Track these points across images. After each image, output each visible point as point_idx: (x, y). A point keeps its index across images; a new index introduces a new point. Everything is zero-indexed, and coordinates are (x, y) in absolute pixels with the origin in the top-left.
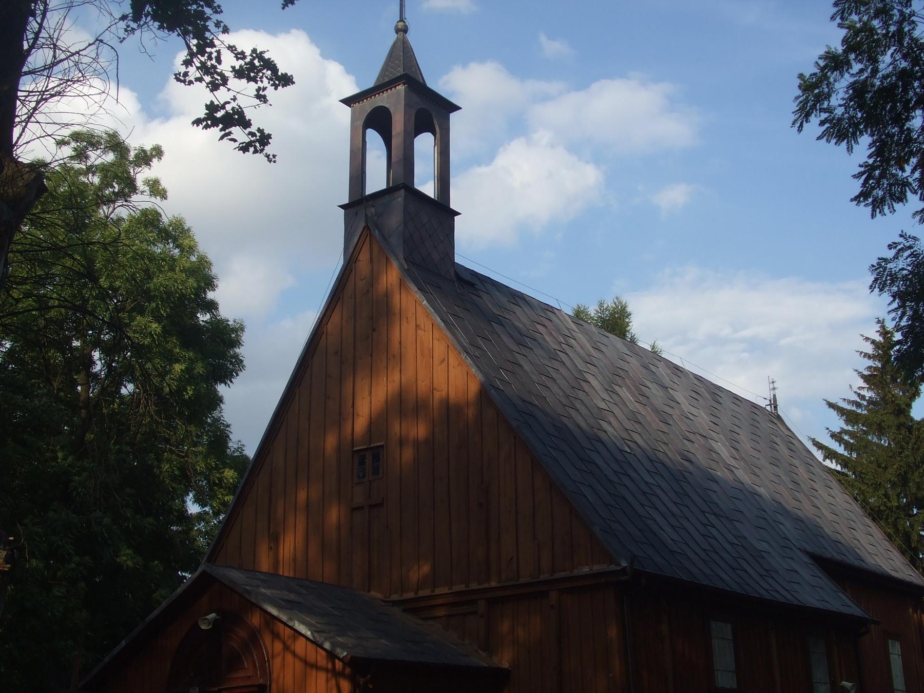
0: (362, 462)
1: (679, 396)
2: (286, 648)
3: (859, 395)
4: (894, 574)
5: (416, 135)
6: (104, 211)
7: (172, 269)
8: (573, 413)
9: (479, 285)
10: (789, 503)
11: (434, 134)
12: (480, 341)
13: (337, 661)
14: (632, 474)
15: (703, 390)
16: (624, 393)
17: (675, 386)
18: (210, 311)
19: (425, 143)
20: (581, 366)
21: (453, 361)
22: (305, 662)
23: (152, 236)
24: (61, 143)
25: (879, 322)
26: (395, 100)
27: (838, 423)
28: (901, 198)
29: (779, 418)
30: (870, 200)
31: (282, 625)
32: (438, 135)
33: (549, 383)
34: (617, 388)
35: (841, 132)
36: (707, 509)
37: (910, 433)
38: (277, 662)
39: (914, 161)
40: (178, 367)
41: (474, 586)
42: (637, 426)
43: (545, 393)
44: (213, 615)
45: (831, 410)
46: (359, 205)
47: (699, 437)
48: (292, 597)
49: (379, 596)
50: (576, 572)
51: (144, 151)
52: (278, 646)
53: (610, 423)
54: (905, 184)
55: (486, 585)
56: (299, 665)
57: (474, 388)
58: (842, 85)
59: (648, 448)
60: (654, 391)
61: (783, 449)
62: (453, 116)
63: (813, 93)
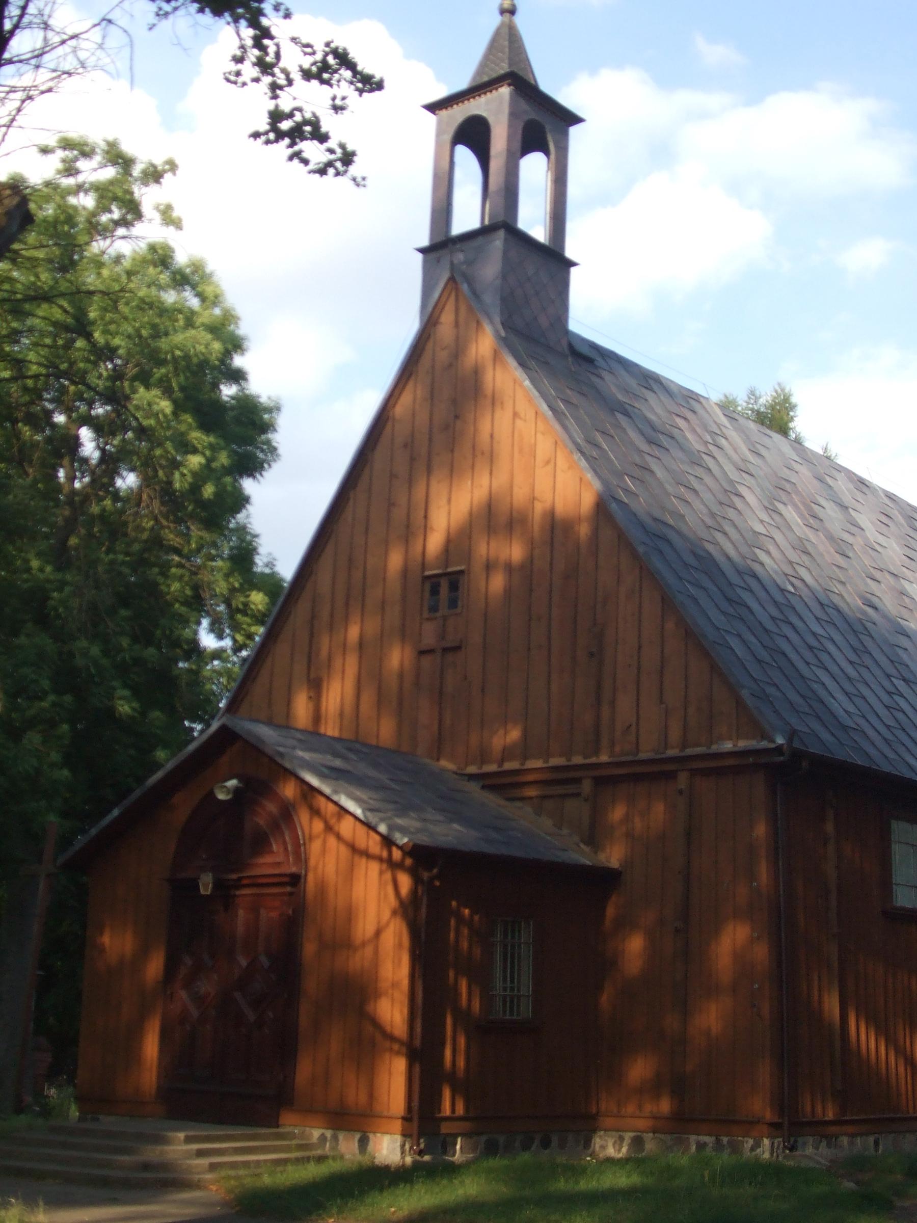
0: (435, 591)
1: (864, 520)
2: (329, 828)
8: (719, 537)
9: (600, 362)
11: (547, 153)
12: (599, 439)
15: (895, 513)
16: (789, 513)
17: (858, 507)
19: (534, 169)
20: (733, 474)
26: (496, 108)
32: (553, 156)
33: (690, 497)
38: (315, 847)
41: (578, 760)
42: (805, 558)
43: (682, 509)
46: (442, 247)
47: (887, 576)
50: (715, 748)
51: (154, 166)
52: (318, 826)
53: (768, 553)
55: (593, 760)
56: (344, 851)
57: (588, 500)
60: (830, 512)
62: (574, 131)
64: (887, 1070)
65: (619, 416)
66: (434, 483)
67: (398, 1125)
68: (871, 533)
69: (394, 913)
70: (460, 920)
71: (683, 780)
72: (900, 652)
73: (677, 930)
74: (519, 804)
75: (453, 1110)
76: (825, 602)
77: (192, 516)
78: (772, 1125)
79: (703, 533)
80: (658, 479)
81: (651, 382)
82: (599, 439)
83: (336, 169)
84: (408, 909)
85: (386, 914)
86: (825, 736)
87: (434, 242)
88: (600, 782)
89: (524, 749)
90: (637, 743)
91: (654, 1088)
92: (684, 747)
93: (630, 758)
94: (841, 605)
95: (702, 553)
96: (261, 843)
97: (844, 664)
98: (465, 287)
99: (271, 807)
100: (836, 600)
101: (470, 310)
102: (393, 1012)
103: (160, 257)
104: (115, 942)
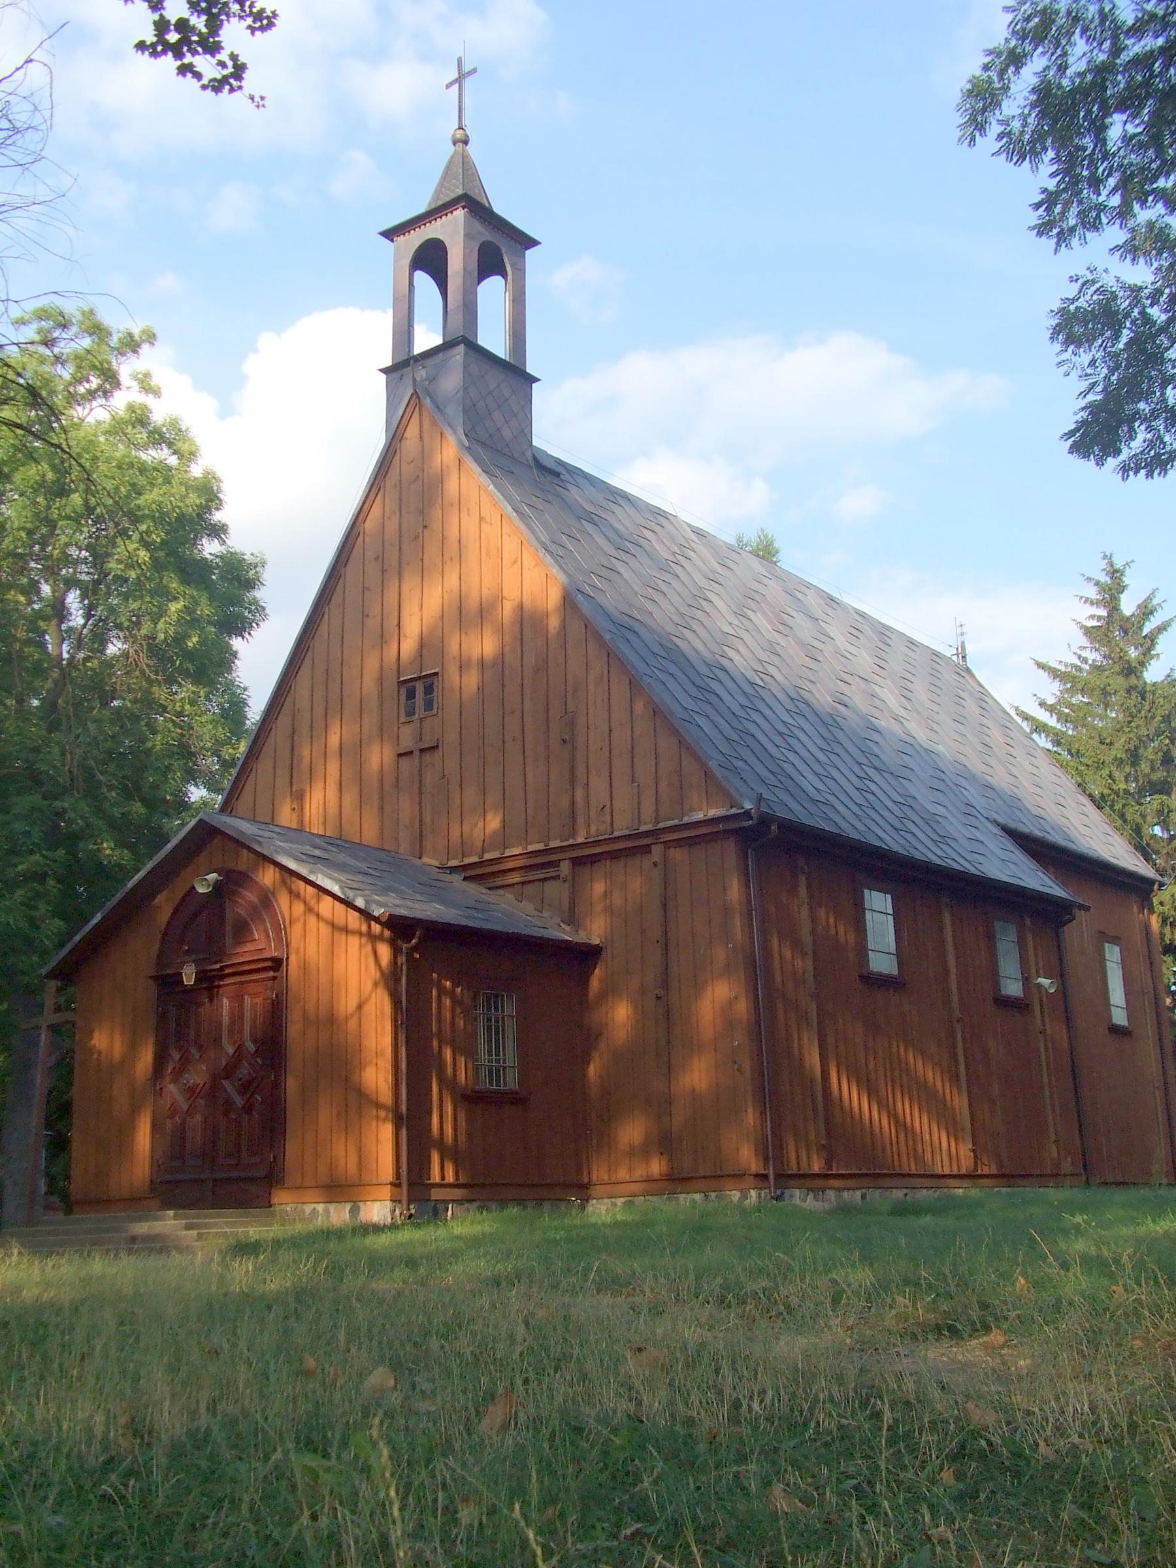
0: (411, 695)
2: (309, 909)
3: (1079, 657)
4: (1113, 860)
5: (480, 281)
6: (79, 411)
7: (168, 481)
9: (565, 476)
10: (976, 765)
11: (505, 276)
12: (565, 540)
13: (373, 923)
15: (865, 628)
16: (758, 619)
17: (828, 619)
18: (218, 536)
19: (492, 294)
20: (702, 582)
21: (528, 561)
22: (333, 925)
23: (142, 436)
24: (21, 322)
25: (1105, 557)
26: (453, 230)
27: (1051, 690)
28: (1095, 226)
29: (968, 670)
30: (1055, 231)
31: (302, 884)
32: (510, 277)
33: (657, 597)
34: (749, 613)
35: (1021, 150)
36: (864, 761)
37: (1143, 699)
38: (296, 932)
39: (1112, 182)
40: (174, 607)
42: (774, 658)
43: (650, 606)
44: (215, 875)
45: (1041, 671)
46: (403, 366)
47: (858, 680)
48: (317, 853)
50: (686, 820)
52: (299, 908)
54: (1101, 208)
55: (571, 842)
56: (325, 930)
57: (554, 597)
59: (787, 683)
60: (800, 622)
61: (971, 706)
62: (530, 254)
63: (983, 99)
64: (872, 1140)
65: (584, 522)
66: (405, 588)
67: (387, 1191)
68: (842, 642)
69: (376, 984)
70: (442, 991)
71: (657, 850)
72: (871, 744)
73: (658, 998)
74: (501, 892)
75: (443, 1178)
76: (795, 696)
78: (756, 1176)
79: (671, 629)
83: (231, 85)
84: (391, 979)
85: (369, 985)
87: (397, 361)
88: (577, 862)
89: (503, 838)
90: (612, 824)
91: (642, 1152)
92: (657, 821)
93: (606, 837)
94: (811, 700)
95: (669, 645)
96: (242, 930)
97: (814, 750)
98: (427, 401)
99: (251, 896)
100: (806, 695)
101: (434, 423)
102: (378, 1077)
103: (139, 418)
104: (106, 1041)
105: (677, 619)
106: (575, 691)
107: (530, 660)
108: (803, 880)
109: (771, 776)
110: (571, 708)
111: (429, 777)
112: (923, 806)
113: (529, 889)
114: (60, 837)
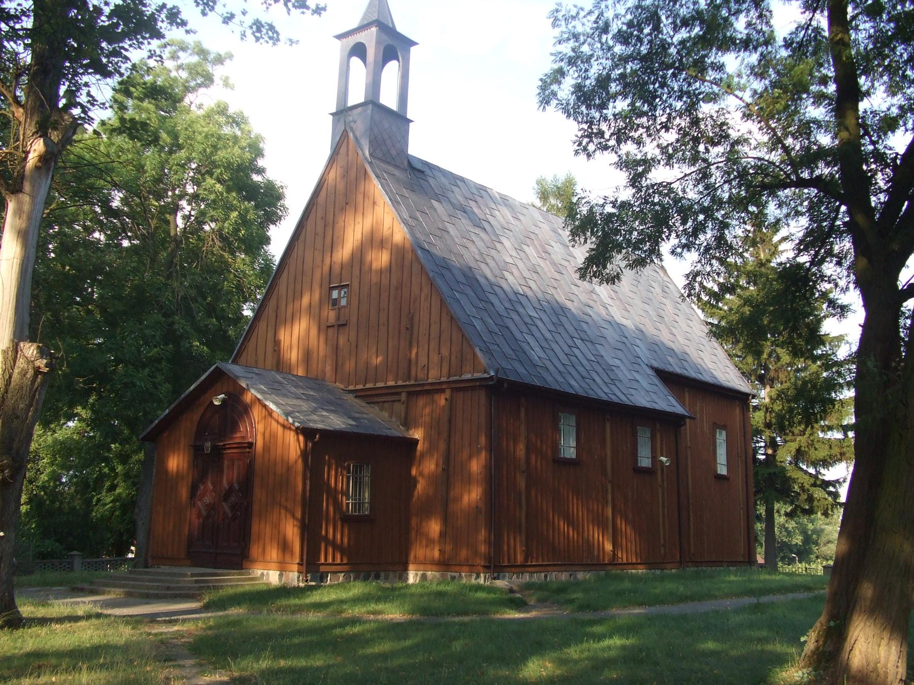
8: (483, 266)
9: (428, 172)
10: (650, 330)
11: (399, 61)
12: (418, 214)
14: (521, 310)
16: (530, 251)
19: (392, 69)
23: (222, 119)
26: (369, 38)
33: (469, 244)
36: (576, 335)
41: (400, 383)
42: (534, 275)
44: (223, 396)
46: (342, 113)
49: (342, 386)
50: (267, 403)
51: (220, 55)
53: (512, 273)
55: (407, 383)
58: (569, 82)
62: (413, 49)
75: (326, 560)
77: (239, 248)
78: (484, 567)
79: (473, 264)
80: (451, 236)
81: (459, 182)
82: (418, 214)
86: (521, 370)
97: (545, 332)
105: (478, 257)
106: (414, 302)
107: (394, 282)
108: (523, 410)
109: (511, 352)
110: (412, 311)
111: (342, 340)
112: (605, 361)
113: (386, 405)
114: (171, 336)
